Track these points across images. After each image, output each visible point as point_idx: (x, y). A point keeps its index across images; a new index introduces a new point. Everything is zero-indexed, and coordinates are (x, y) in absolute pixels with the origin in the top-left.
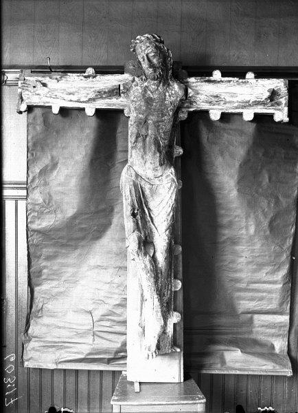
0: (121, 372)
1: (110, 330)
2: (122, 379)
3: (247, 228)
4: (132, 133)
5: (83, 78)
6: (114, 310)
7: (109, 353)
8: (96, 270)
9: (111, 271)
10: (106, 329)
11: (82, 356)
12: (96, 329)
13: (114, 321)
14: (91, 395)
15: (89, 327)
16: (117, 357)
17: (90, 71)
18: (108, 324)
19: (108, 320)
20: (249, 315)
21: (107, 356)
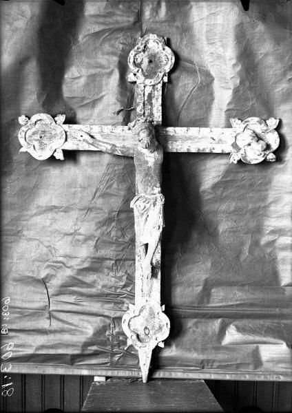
0: (92, 377)
1: (75, 308)
2: (93, 391)
3: (242, 179)
4: (157, 99)
5: (62, 214)
6: (80, 277)
7: (73, 346)
8: (50, 215)
9: (74, 214)
10: (69, 307)
11: (30, 351)
12: (55, 308)
13: (81, 294)
14: (47, 399)
15: (42, 304)
16: (86, 352)
17: (162, 345)
18: (72, 299)
19: (73, 293)
20: (255, 345)
21: (70, 351)
